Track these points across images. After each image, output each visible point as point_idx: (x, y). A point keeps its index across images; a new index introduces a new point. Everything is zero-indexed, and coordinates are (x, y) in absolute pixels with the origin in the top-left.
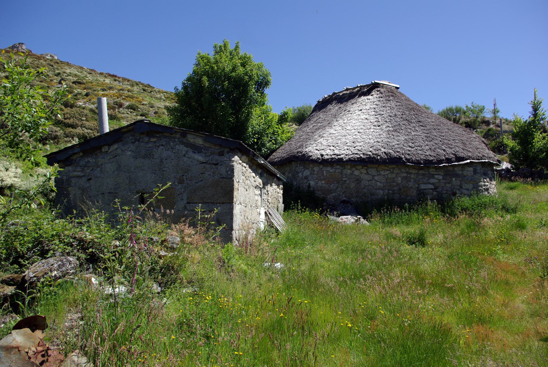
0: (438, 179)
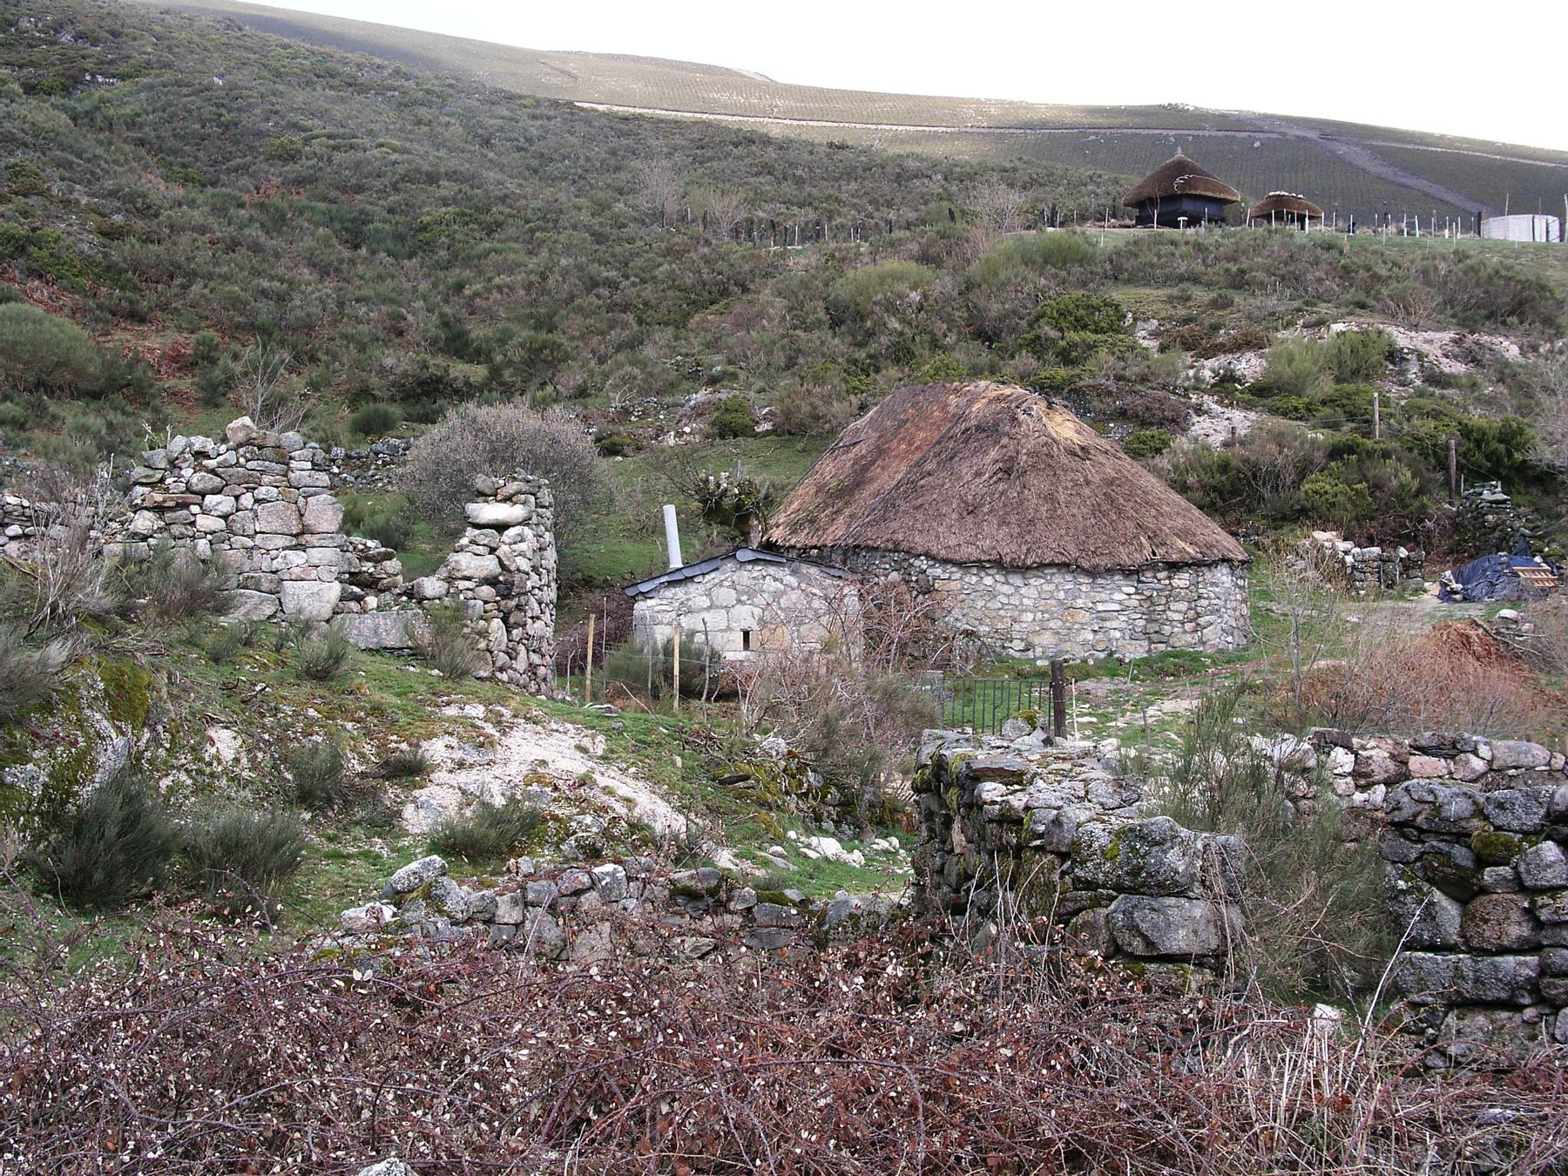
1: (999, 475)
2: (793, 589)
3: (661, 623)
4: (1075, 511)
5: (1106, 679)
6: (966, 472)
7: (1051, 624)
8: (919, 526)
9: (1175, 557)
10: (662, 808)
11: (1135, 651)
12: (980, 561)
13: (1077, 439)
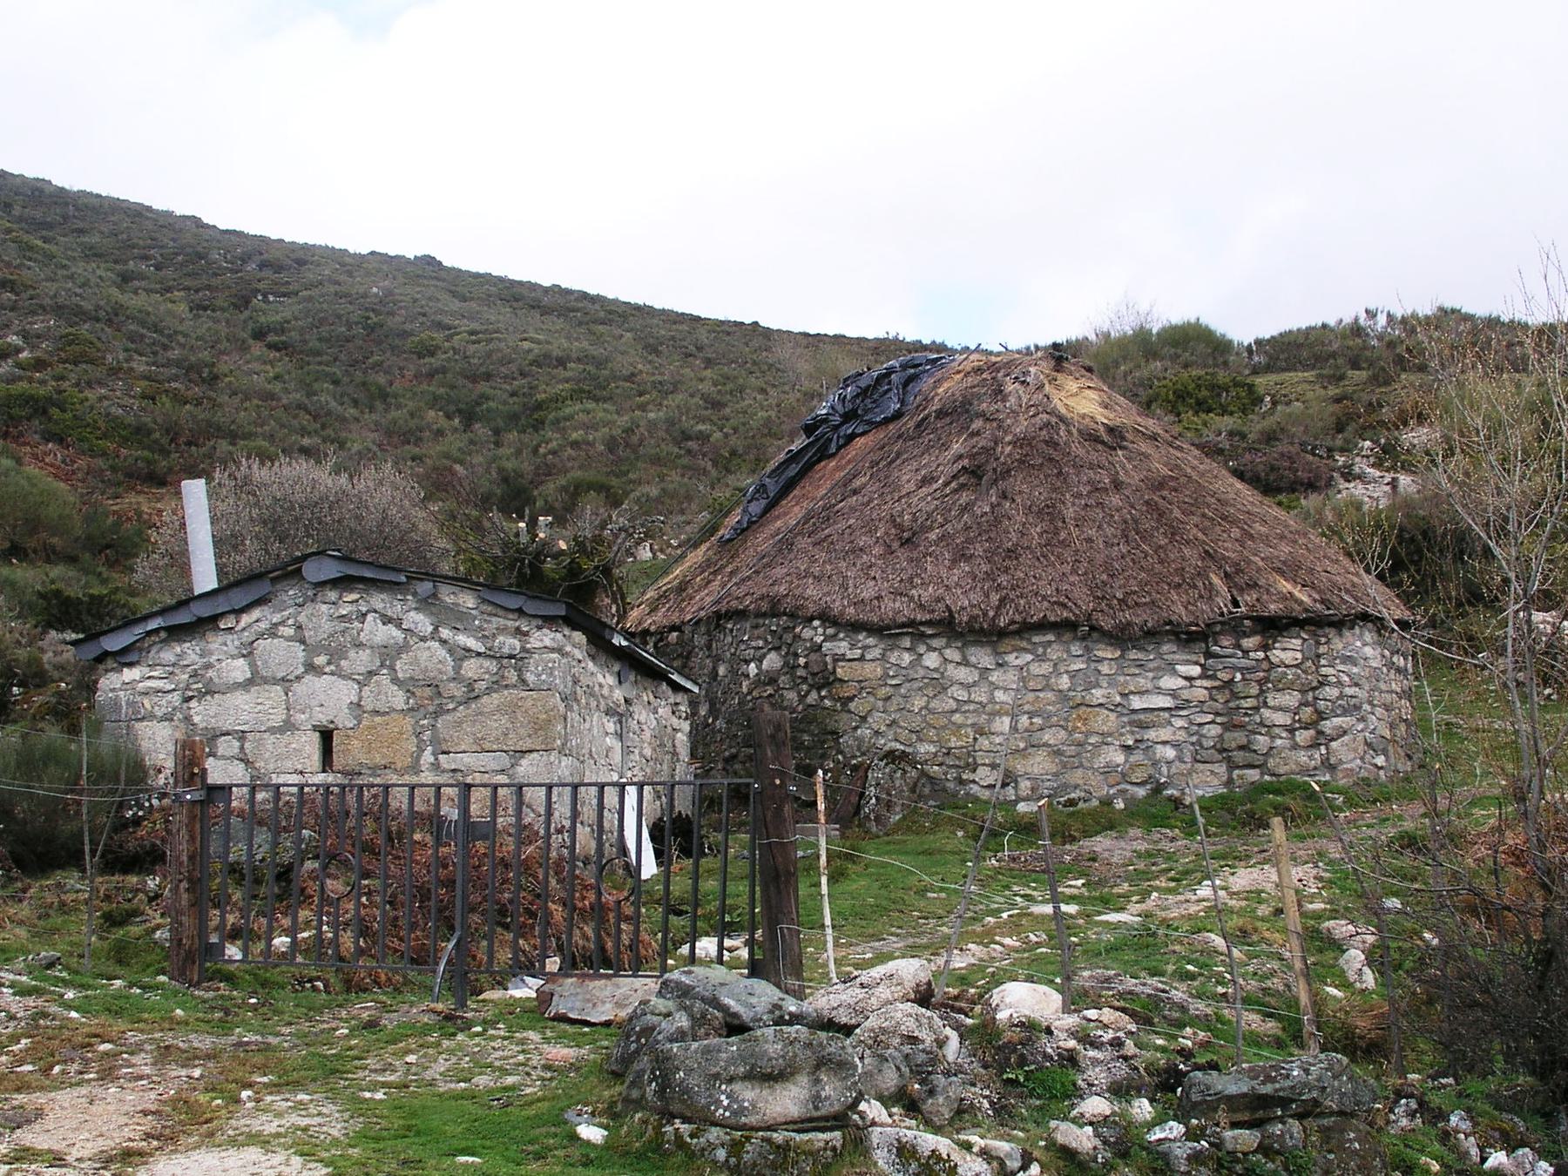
0: (1186, 678)
1: (962, 480)
2: (423, 639)
3: (150, 716)
4: (1092, 533)
5: (1137, 832)
6: (907, 477)
7: (1047, 737)
8: (816, 570)
9: (1273, 608)
10: (566, 1051)
11: (1206, 783)
12: (912, 623)
13: (1102, 415)
